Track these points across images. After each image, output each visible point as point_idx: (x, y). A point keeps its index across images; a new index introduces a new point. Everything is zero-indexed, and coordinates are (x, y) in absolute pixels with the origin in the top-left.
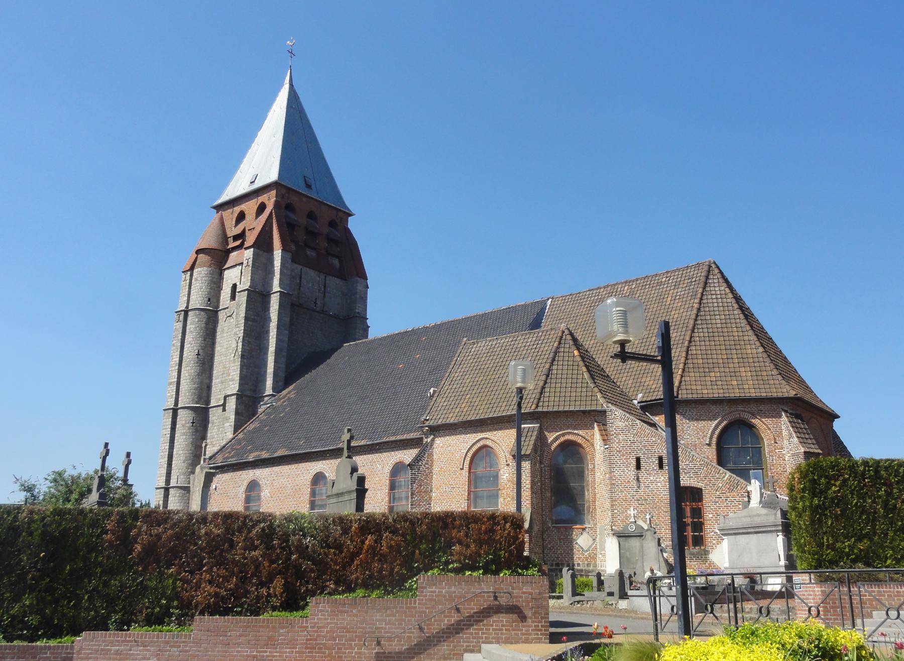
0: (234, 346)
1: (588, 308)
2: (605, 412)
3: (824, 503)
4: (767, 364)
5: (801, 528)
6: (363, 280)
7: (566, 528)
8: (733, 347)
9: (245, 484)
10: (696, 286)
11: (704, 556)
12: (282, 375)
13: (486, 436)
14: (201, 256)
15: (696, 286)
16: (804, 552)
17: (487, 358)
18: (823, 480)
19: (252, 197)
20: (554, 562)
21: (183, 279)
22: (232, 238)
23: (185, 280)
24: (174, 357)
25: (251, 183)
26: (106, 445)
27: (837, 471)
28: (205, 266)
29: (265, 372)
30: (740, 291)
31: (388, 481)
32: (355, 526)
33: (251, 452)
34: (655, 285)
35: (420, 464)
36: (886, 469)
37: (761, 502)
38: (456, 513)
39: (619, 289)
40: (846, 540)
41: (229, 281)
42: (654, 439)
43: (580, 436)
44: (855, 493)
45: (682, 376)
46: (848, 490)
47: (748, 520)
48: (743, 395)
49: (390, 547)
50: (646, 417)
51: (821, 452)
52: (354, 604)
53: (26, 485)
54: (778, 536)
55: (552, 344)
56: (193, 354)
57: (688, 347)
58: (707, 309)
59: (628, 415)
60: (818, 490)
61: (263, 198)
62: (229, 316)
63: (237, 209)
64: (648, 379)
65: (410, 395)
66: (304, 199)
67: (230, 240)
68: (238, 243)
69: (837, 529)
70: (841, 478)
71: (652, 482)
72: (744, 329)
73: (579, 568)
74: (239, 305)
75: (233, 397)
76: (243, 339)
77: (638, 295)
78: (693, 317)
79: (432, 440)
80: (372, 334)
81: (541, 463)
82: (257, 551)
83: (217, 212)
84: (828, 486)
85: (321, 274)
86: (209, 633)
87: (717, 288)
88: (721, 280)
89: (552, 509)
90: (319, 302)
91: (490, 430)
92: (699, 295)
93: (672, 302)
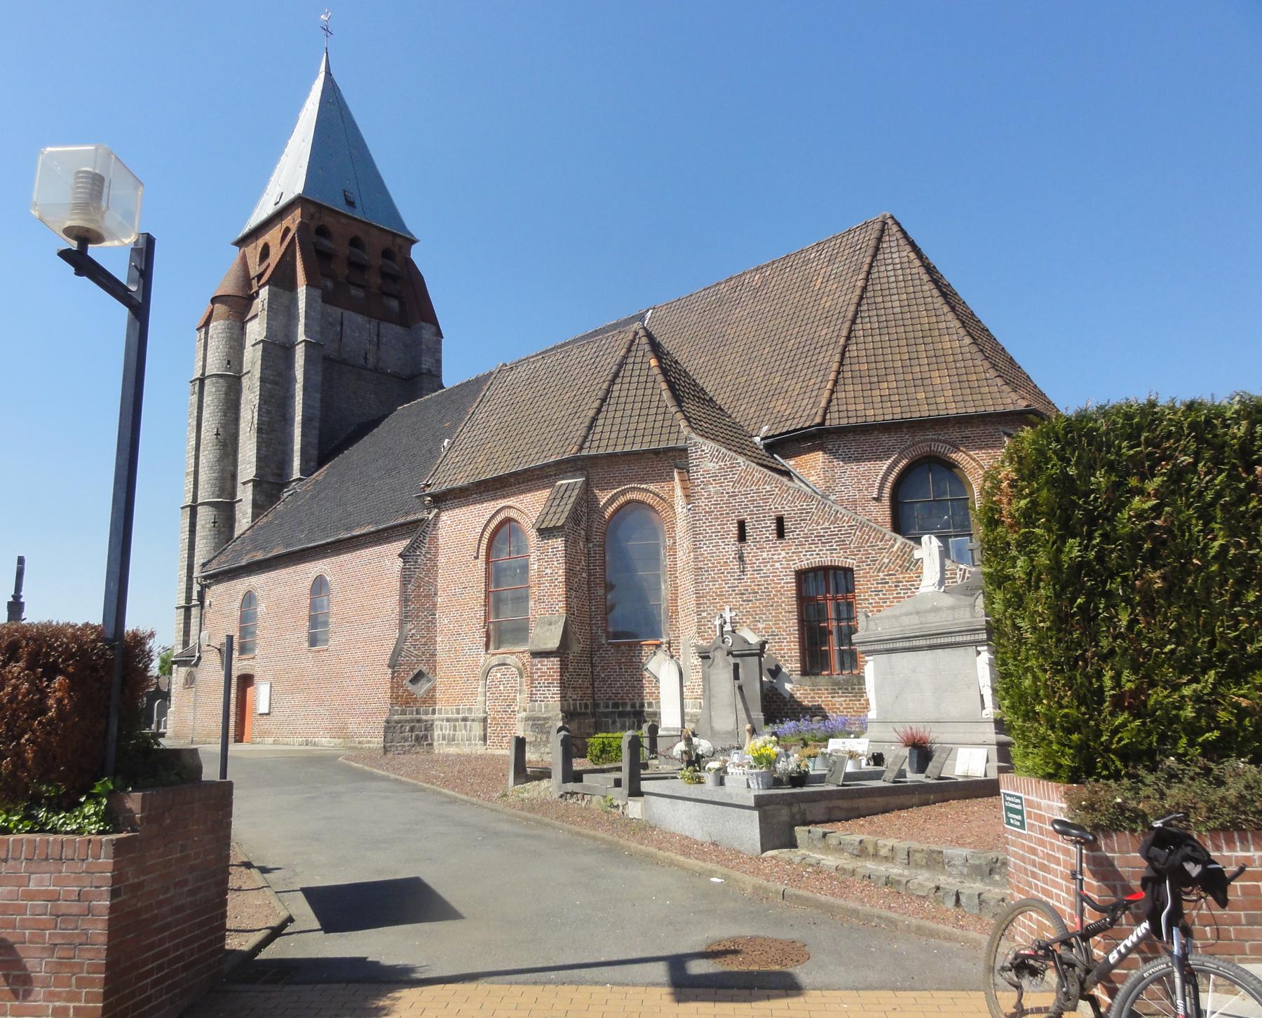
0: (250, 417)
2: (685, 450)
3: (1100, 558)
4: (978, 362)
5: (1021, 641)
6: (429, 325)
7: (629, 644)
8: (921, 341)
10: (861, 256)
11: (857, 687)
12: (314, 453)
13: (508, 504)
15: (861, 256)
16: (1030, 715)
18: (1100, 478)
23: (200, 340)
27: (1148, 443)
29: (292, 450)
30: (933, 260)
31: (398, 583)
35: (418, 553)
37: (941, 582)
38: (38, 629)
39: (747, 281)
40: (1185, 679)
42: (768, 488)
43: (651, 492)
44: (1219, 514)
45: (832, 392)
46: (1189, 506)
47: (915, 620)
50: (772, 460)
54: (979, 653)
57: (845, 346)
59: (723, 450)
60: (1079, 514)
63: (261, 242)
64: (780, 402)
69: (1150, 642)
70: (1166, 467)
71: (765, 562)
73: (650, 710)
76: (259, 407)
77: (772, 284)
78: (855, 300)
79: (435, 516)
81: (588, 540)
84: (1119, 494)
87: (896, 252)
88: (902, 242)
89: (606, 614)
90: (371, 359)
91: (514, 494)
92: (866, 268)
93: (824, 285)
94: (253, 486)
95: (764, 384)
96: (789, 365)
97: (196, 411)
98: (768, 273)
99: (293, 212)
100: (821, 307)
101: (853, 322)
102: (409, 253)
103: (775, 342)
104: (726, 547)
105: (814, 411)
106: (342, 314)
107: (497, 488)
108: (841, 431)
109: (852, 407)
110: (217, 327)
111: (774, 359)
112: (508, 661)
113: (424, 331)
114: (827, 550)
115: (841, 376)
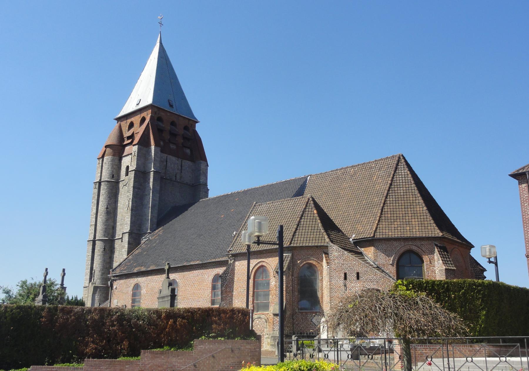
0: (127, 203)
1: (330, 182)
2: (327, 247)
4: (428, 217)
6: (205, 162)
7: (306, 313)
9: (133, 286)
12: (155, 220)
14: (108, 149)
17: (266, 214)
19: (138, 113)
20: (299, 332)
21: (98, 163)
22: (126, 138)
23: (99, 164)
24: (93, 209)
25: (137, 104)
26: (47, 269)
28: (110, 155)
32: (164, 315)
33: (136, 267)
34: (368, 168)
35: (227, 276)
36: (438, 285)
39: (348, 171)
41: (125, 164)
42: (354, 263)
45: (378, 224)
48: (412, 235)
49: (180, 325)
51: (455, 269)
52: (162, 353)
53: (6, 290)
55: (302, 206)
56: (104, 208)
58: (396, 184)
61: (144, 114)
62: (125, 185)
63: (129, 121)
64: (359, 226)
65: (225, 234)
66: (168, 114)
67: (126, 139)
68: (129, 141)
71: (353, 287)
72: (417, 196)
73: (313, 335)
74: (130, 180)
75: (127, 234)
76: (132, 199)
77: (358, 174)
78: (387, 189)
79: (233, 262)
80: (212, 195)
81: (292, 276)
82: (115, 327)
83: (118, 123)
85: (179, 159)
86: (91, 367)
88: (405, 166)
89: (298, 302)
90: (178, 177)
92: (392, 176)
94: (129, 235)
95: (354, 217)
96: (363, 211)
97: (97, 196)
98: (356, 169)
99: (147, 110)
100: (376, 188)
101: (386, 197)
102: (195, 128)
103: (358, 201)
104: (340, 281)
105: (371, 231)
106: (167, 157)
107: (258, 254)
108: (380, 240)
109: (384, 231)
110: (107, 159)
111: (358, 207)
112: (261, 317)
113: (202, 165)
114: (373, 284)
115: (381, 218)
